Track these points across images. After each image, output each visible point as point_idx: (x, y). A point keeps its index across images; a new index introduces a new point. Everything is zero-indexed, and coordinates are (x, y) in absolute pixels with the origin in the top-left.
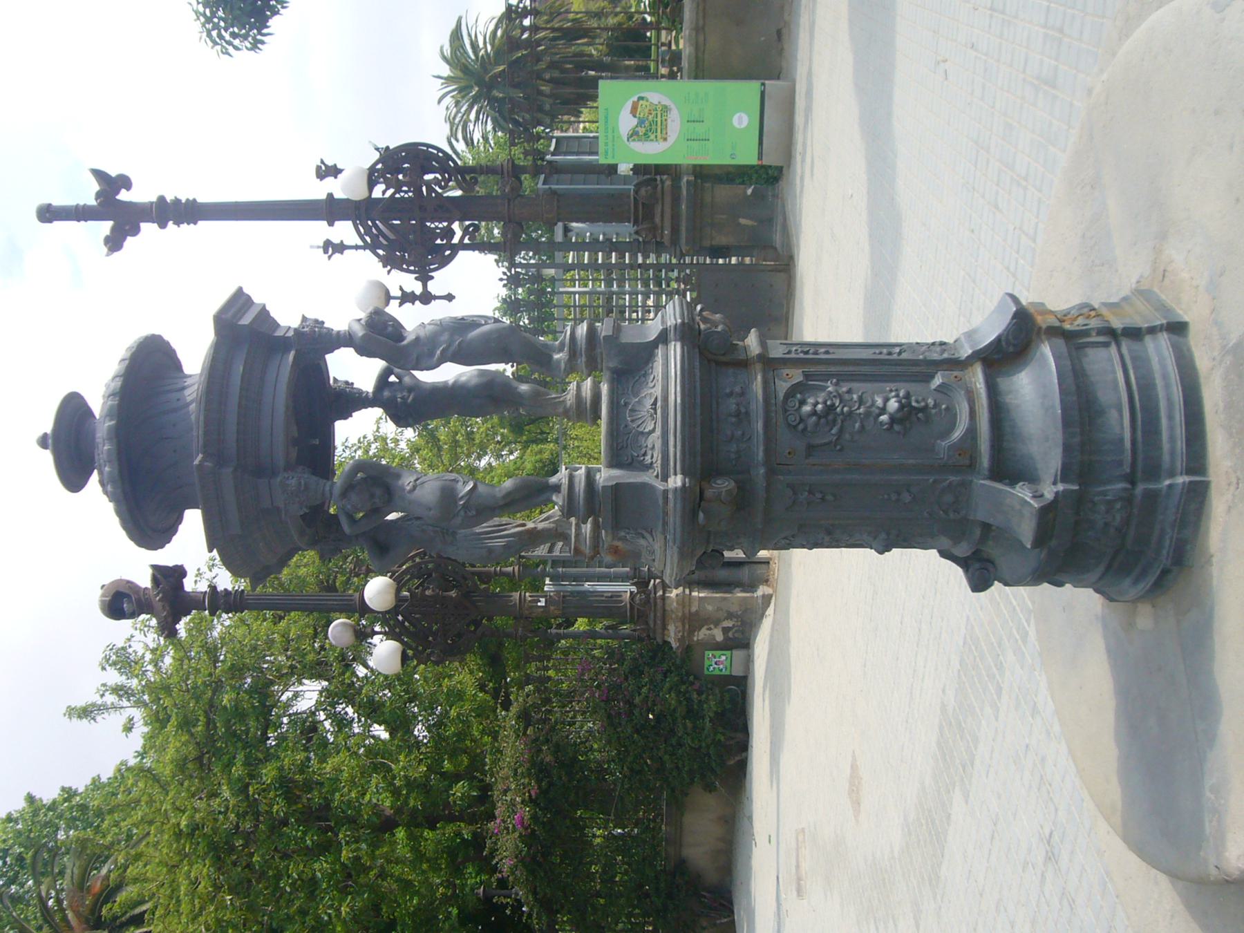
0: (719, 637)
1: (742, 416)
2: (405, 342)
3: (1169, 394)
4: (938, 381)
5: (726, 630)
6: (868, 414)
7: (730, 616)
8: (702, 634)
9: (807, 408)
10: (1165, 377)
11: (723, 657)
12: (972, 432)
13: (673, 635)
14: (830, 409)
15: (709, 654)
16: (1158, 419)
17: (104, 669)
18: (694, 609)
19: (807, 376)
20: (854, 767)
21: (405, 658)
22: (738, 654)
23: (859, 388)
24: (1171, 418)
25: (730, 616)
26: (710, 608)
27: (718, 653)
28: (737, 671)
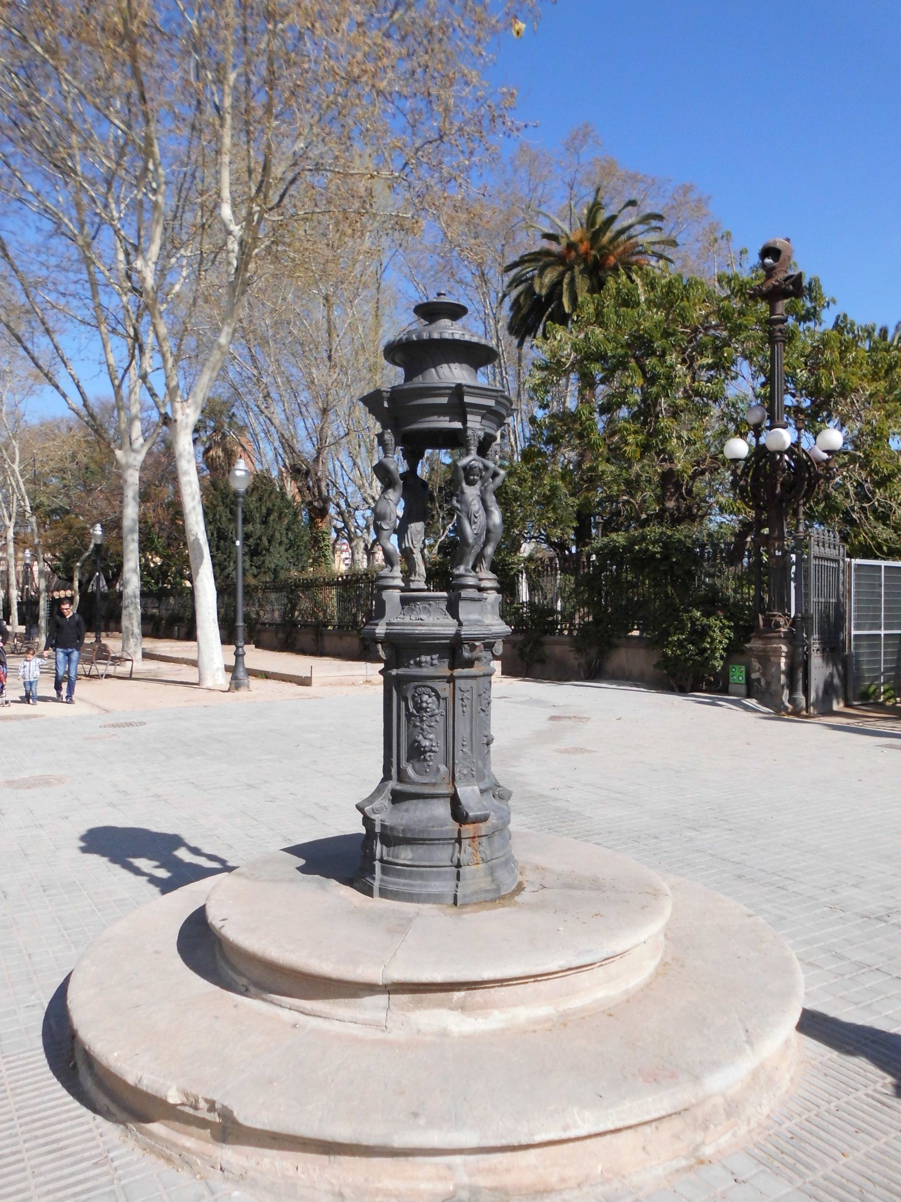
0: (754, 676)
1: (419, 664)
2: (464, 485)
3: (417, 886)
4: (443, 768)
5: (758, 680)
6: (422, 729)
7: (768, 684)
8: (756, 665)
9: (425, 698)
10: (426, 886)
11: (742, 679)
12: (413, 783)
13: (755, 644)
14: (425, 710)
15: (743, 669)
16: (406, 878)
17: (770, 251)
18: (772, 659)
19: (445, 699)
20: (589, 751)
21: (735, 461)
22: (743, 689)
23: (441, 727)
24: (404, 885)
25: (768, 684)
26: (773, 670)
27: (744, 674)
28: (731, 688)
